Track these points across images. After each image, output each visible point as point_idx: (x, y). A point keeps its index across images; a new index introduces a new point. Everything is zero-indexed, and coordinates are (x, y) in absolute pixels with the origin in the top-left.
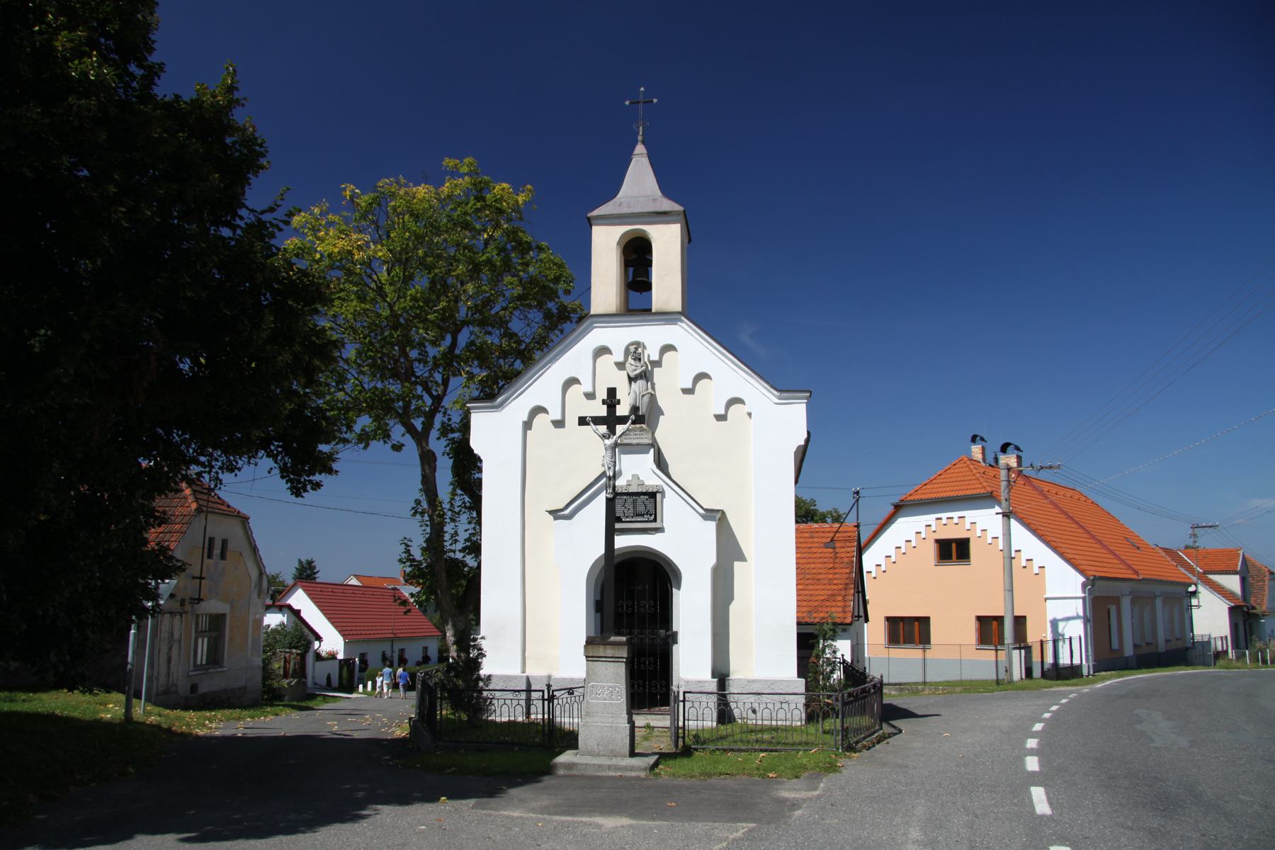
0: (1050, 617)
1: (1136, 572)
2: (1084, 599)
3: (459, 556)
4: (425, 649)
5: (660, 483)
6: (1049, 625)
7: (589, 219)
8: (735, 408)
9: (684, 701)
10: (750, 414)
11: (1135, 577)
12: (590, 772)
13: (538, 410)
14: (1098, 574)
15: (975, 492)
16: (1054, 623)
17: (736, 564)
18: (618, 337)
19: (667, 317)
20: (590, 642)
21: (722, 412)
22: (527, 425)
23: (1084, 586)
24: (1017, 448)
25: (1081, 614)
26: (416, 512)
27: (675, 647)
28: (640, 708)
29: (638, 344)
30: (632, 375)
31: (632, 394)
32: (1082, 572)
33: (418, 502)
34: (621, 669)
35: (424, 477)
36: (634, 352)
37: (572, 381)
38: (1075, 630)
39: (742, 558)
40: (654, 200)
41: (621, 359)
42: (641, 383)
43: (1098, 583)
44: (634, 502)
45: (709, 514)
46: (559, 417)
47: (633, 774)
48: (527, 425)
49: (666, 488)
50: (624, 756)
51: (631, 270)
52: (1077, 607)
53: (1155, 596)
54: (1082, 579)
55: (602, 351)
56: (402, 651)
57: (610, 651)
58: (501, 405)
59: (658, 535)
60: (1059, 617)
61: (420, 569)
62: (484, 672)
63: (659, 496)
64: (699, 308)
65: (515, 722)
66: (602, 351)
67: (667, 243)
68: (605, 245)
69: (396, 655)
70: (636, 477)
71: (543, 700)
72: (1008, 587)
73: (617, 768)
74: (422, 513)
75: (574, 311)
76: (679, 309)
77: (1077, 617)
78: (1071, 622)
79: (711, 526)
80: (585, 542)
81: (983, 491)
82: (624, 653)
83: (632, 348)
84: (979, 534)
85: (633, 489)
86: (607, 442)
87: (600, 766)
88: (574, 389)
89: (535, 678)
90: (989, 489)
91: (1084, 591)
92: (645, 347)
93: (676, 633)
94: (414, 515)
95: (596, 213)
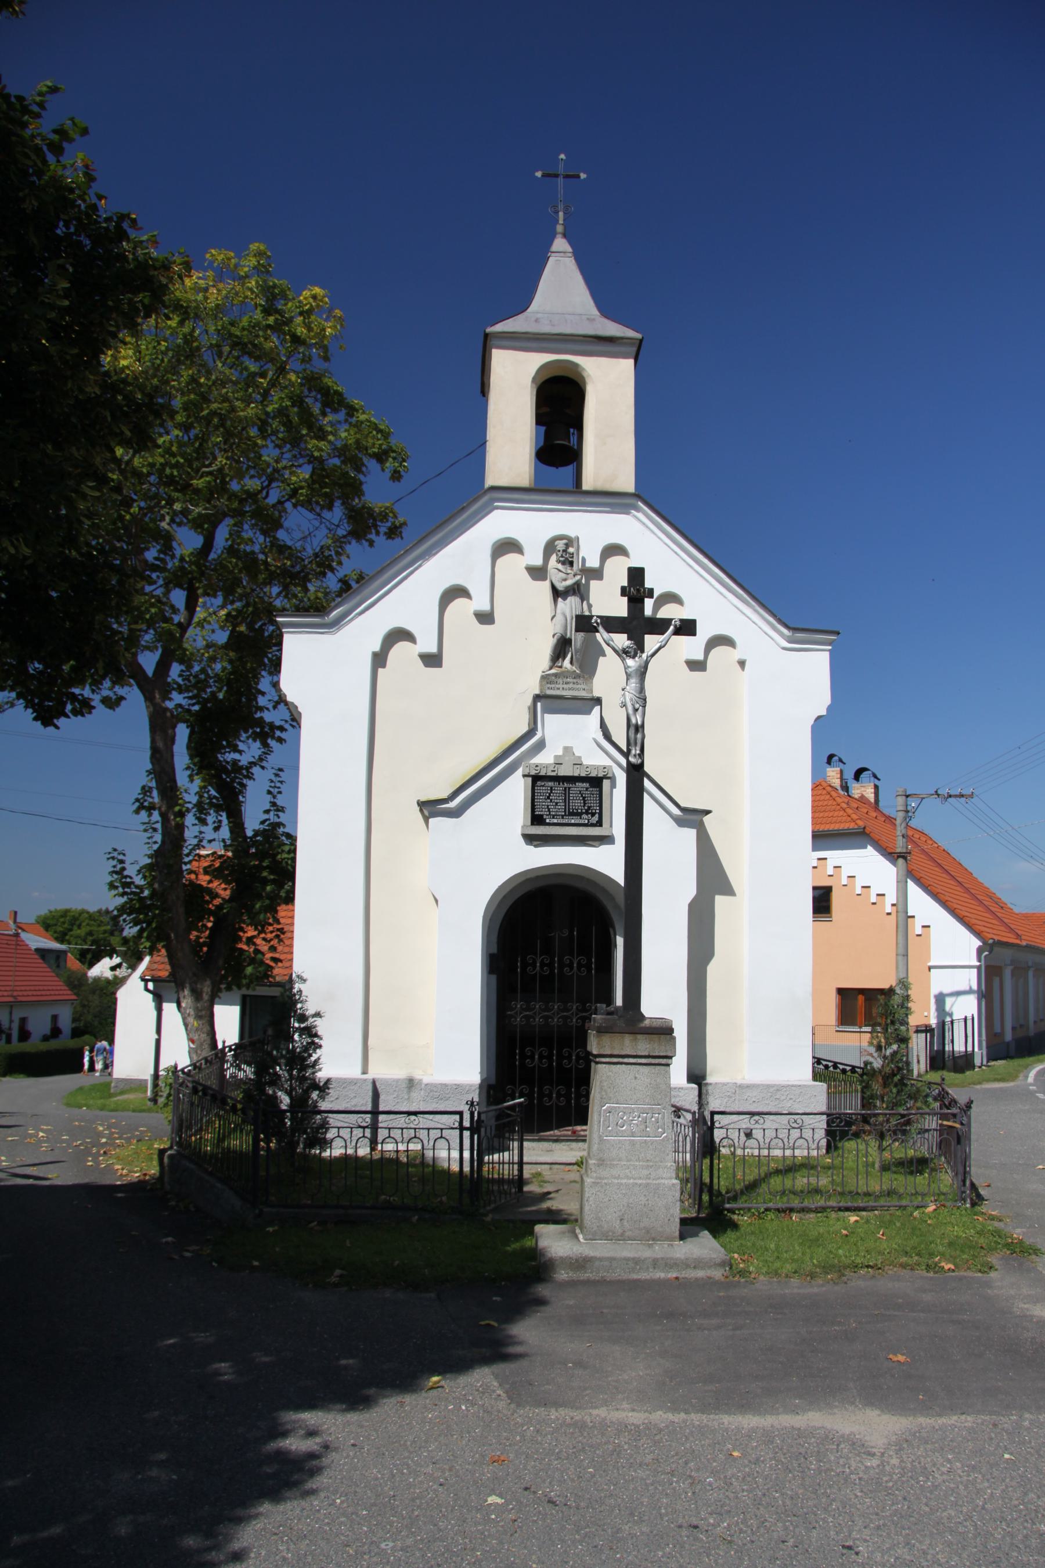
0: (934, 990)
1: (1018, 936)
2: (979, 968)
3: (204, 880)
4: (55, 1018)
5: (608, 762)
6: (933, 1001)
7: (486, 336)
10: (742, 664)
11: (1017, 941)
12: (619, 1274)
13: (399, 635)
14: (996, 938)
15: (842, 826)
16: (940, 999)
17: (718, 899)
18: (534, 526)
19: (609, 500)
21: (700, 657)
22: (379, 660)
23: (980, 951)
24: (875, 776)
25: (975, 987)
26: (142, 807)
28: (531, 1131)
29: (570, 542)
30: (561, 586)
31: (559, 618)
32: (978, 934)
33: (146, 790)
35: (155, 751)
36: (562, 549)
37: (456, 593)
38: (966, 1008)
39: (728, 890)
40: (591, 320)
41: (538, 561)
42: (573, 601)
43: (996, 949)
46: (433, 649)
47: (700, 1274)
48: (379, 660)
52: (970, 979)
53: (1029, 967)
54: (978, 943)
55: (507, 547)
56: (23, 1021)
58: (335, 625)
60: (946, 991)
61: (142, 900)
62: (322, 1075)
63: (606, 784)
64: (658, 489)
65: (356, 1158)
66: (507, 547)
67: (610, 390)
68: (513, 380)
69: (15, 1026)
71: (462, 1128)
72: (901, 951)
73: (669, 1264)
74: (150, 809)
75: (384, 517)
76: (630, 488)
77: (970, 992)
78: (961, 998)
80: (499, 847)
81: (852, 825)
83: (560, 545)
84: (844, 881)
85: (564, 771)
86: (630, 662)
87: (637, 1261)
88: (458, 605)
89: (389, 1083)
90: (861, 823)
91: (979, 960)
94: (137, 812)
95: (499, 328)
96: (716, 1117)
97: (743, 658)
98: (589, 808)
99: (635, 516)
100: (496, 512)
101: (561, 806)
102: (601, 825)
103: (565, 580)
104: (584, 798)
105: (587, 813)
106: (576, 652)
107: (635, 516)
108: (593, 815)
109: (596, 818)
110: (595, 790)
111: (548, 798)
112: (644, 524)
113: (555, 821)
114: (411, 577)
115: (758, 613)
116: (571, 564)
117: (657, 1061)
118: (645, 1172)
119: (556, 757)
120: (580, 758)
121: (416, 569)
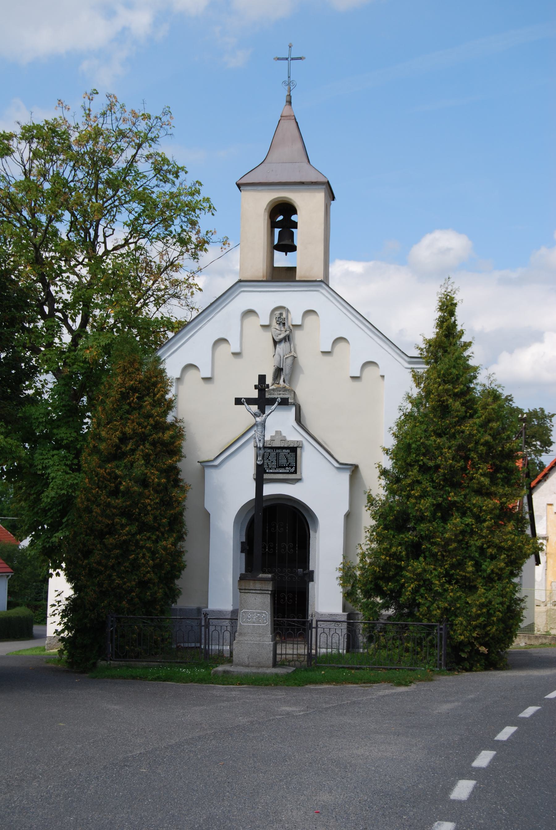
8: (370, 370)
9: (317, 628)
10: (383, 377)
20: (242, 578)
27: (311, 584)
34: (267, 600)
36: (280, 315)
44: (277, 455)
45: (343, 466)
49: (305, 444)
50: (268, 667)
51: (277, 231)
57: (258, 585)
59: (298, 485)
63: (298, 450)
70: (278, 433)
79: (345, 477)
82: (269, 587)
85: (277, 444)
88: (223, 347)
92: (288, 311)
93: (313, 572)
96: (319, 623)
97: (382, 374)
98: (290, 463)
99: (321, 293)
100: (242, 294)
101: (275, 463)
102: (296, 473)
103: (280, 334)
104: (287, 458)
105: (288, 466)
106: (286, 375)
107: (321, 293)
108: (292, 467)
109: (293, 469)
110: (293, 454)
111: (268, 458)
112: (327, 297)
113: (271, 471)
114: (188, 343)
115: (392, 348)
116: (284, 324)
117: (264, 592)
118: (258, 638)
119: (271, 436)
120: (285, 437)
121: (199, 329)
